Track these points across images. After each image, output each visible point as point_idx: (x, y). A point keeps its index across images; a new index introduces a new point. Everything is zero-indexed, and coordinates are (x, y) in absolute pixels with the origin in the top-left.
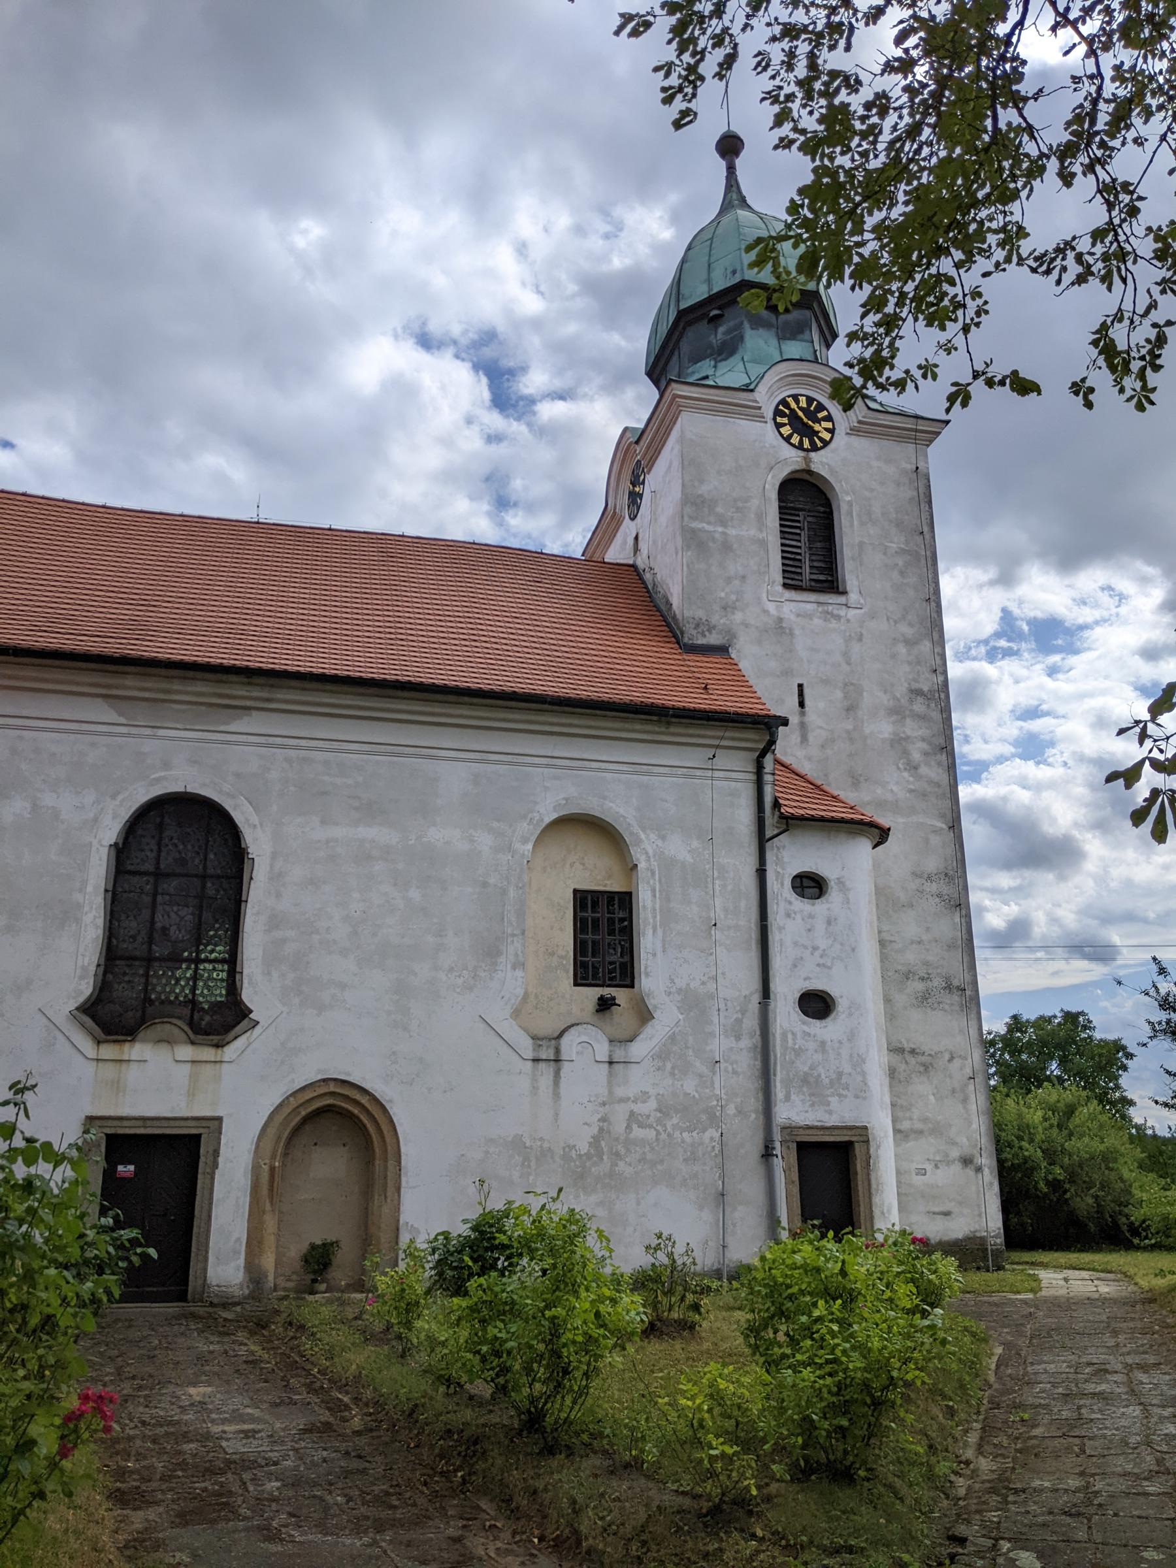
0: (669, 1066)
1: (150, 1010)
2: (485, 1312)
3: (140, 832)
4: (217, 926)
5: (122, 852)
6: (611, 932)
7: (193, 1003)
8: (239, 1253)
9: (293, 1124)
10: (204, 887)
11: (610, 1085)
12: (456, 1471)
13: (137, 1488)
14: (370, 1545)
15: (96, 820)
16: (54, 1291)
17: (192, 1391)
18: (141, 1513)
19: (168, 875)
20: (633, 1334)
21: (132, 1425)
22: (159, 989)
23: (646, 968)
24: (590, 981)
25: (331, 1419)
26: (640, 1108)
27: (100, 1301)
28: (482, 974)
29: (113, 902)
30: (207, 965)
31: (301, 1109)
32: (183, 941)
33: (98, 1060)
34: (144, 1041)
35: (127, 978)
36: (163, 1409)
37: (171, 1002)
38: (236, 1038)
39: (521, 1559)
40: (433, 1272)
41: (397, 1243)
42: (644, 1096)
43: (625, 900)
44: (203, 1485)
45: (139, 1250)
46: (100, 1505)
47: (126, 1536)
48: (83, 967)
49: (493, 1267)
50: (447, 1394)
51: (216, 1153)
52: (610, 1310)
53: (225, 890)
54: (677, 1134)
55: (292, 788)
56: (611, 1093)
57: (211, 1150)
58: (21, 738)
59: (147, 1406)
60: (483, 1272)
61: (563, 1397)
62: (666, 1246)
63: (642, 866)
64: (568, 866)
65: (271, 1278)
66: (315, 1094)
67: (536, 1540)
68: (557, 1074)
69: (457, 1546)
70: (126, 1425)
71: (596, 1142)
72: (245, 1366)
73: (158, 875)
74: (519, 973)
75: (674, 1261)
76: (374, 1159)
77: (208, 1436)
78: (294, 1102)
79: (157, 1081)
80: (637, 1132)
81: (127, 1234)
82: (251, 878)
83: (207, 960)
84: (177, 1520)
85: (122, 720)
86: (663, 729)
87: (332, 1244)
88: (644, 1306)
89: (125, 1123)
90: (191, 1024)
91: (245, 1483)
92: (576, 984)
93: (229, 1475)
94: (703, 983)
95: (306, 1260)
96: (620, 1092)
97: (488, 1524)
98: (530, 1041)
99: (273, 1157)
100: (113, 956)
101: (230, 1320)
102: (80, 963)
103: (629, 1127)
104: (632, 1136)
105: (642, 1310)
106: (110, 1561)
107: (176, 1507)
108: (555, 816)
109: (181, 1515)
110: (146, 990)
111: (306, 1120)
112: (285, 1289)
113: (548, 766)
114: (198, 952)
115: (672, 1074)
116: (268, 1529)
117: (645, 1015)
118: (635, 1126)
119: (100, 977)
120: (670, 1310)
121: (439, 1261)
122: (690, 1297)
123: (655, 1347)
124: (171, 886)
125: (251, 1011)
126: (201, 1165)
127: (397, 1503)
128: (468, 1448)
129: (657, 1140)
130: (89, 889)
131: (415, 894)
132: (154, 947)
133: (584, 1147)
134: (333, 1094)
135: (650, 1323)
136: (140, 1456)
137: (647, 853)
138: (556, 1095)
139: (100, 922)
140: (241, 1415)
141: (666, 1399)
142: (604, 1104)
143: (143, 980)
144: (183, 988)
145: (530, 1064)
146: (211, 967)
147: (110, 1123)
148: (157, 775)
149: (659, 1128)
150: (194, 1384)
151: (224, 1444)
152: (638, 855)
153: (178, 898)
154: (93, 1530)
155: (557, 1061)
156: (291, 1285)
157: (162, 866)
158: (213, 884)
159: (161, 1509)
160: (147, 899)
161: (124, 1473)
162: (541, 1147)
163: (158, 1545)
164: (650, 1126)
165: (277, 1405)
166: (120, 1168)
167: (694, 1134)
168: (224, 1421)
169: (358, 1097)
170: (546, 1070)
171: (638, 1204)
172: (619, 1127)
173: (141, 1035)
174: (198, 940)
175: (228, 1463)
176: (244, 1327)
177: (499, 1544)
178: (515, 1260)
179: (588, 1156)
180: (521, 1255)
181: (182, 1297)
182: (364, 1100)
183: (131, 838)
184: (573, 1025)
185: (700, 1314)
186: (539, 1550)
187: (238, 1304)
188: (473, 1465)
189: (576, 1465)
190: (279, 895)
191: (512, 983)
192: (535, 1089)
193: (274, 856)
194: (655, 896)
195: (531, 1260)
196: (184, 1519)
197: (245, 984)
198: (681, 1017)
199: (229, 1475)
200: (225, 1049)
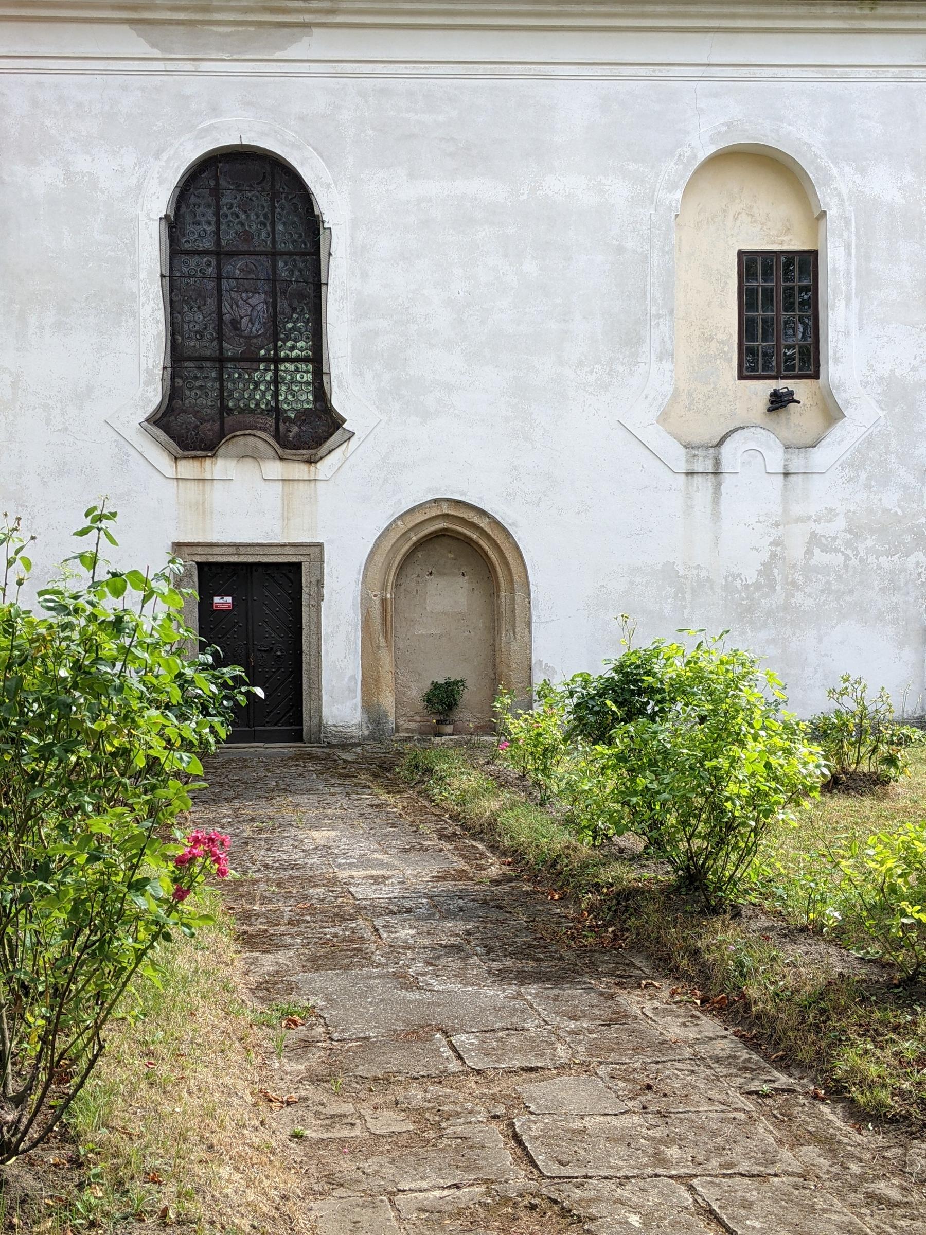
0: (863, 475)
1: (229, 420)
2: (633, 761)
3: (193, 199)
4: (295, 316)
5: (174, 226)
6: (789, 307)
7: (276, 411)
8: (355, 691)
9: (404, 550)
10: (274, 267)
11: (785, 500)
12: (606, 926)
13: (265, 931)
14: (514, 998)
15: (140, 186)
16: (152, 733)
17: (315, 834)
18: (270, 957)
19: (231, 254)
20: (813, 788)
21: (254, 868)
22: (236, 395)
23: (835, 352)
24: (760, 372)
25: (467, 867)
26: (820, 529)
27: (208, 742)
28: (620, 369)
29: (171, 291)
30: (287, 365)
31: (412, 534)
32: (256, 337)
33: (177, 479)
34: (225, 457)
35: (199, 383)
36: (287, 852)
37: (252, 411)
38: (330, 452)
39: (681, 1020)
40: (572, 717)
41: (530, 684)
42: (831, 513)
43: (805, 264)
44: (333, 930)
45: (243, 689)
46: (228, 947)
47: (258, 979)
48: (147, 370)
49: (641, 711)
50: (594, 845)
51: (320, 584)
52: (782, 761)
53: (300, 271)
54: (872, 559)
55: (370, 132)
56: (786, 511)
57: (314, 581)
58: (40, 84)
59: (269, 849)
60: (629, 718)
61: (727, 854)
62: (855, 690)
63: (832, 213)
64: (730, 218)
65: (392, 718)
66: (427, 517)
67: (698, 1002)
68: (717, 487)
69: (610, 1003)
70: (248, 868)
71: (766, 569)
72: (370, 810)
73: (220, 254)
74: (667, 365)
75: (865, 708)
76: (499, 591)
77: (333, 881)
78: (402, 527)
79: (247, 502)
80: (820, 558)
81: (230, 671)
82: (330, 254)
83: (287, 359)
84: (309, 964)
85: (157, 53)
86: (867, 11)
87: (456, 683)
88: (826, 758)
89: (217, 550)
90: (277, 436)
91: (377, 930)
92: (741, 377)
93: (360, 921)
94: (914, 369)
95: (429, 699)
96: (797, 509)
97: (644, 982)
98: (684, 450)
99: (384, 588)
100: (178, 356)
101: (350, 762)
102: (143, 367)
103: (809, 552)
104: (812, 562)
105: (823, 762)
106: (243, 1001)
107: (306, 951)
108: (711, 150)
109: (313, 959)
110: (221, 397)
111: (419, 545)
112: (407, 730)
113: (701, 78)
114: (276, 349)
115: (868, 486)
116: (405, 977)
117: (832, 413)
118: (817, 551)
119: (168, 382)
120: (858, 763)
121: (578, 705)
122: (883, 748)
123: (839, 804)
124: (235, 267)
125: (344, 421)
126: (305, 597)
127: (542, 956)
128: (619, 903)
129: (846, 566)
130: (143, 275)
131: (530, 267)
132: (225, 344)
133: (751, 575)
134: (446, 516)
135: (833, 776)
136: (265, 900)
137: (839, 195)
138: (716, 516)
139: (160, 315)
140: (369, 860)
141: (851, 862)
142: (777, 525)
143: (217, 385)
144: (264, 394)
145: (683, 476)
146: (293, 368)
147: (199, 550)
148: (205, 124)
149: (849, 552)
150: (316, 828)
151: (353, 889)
152: (827, 198)
153: (244, 285)
154: (225, 971)
155: (716, 473)
156: (413, 726)
157: (223, 243)
158: (286, 263)
159: (291, 953)
160: (212, 285)
161: (250, 916)
162: (698, 575)
163: (290, 988)
164: (837, 550)
165: (406, 851)
166: (217, 600)
167: (895, 558)
168: (351, 866)
169: (476, 520)
170: (704, 485)
171: (820, 640)
172: (796, 551)
173: (222, 451)
174: (275, 334)
175: (359, 909)
176: (368, 769)
177: (656, 1004)
178: (666, 706)
179: (758, 586)
180: (673, 700)
181: (298, 737)
182: (484, 524)
183: (183, 209)
184: (736, 430)
185: (897, 767)
186: (702, 1012)
187: (358, 745)
188: (625, 921)
189: (743, 926)
190: (365, 275)
191: (657, 378)
192: (689, 508)
193: (355, 224)
194: (849, 254)
195: (687, 705)
196: (315, 963)
197: (334, 384)
198: (882, 414)
199: (360, 921)
200: (319, 465)
